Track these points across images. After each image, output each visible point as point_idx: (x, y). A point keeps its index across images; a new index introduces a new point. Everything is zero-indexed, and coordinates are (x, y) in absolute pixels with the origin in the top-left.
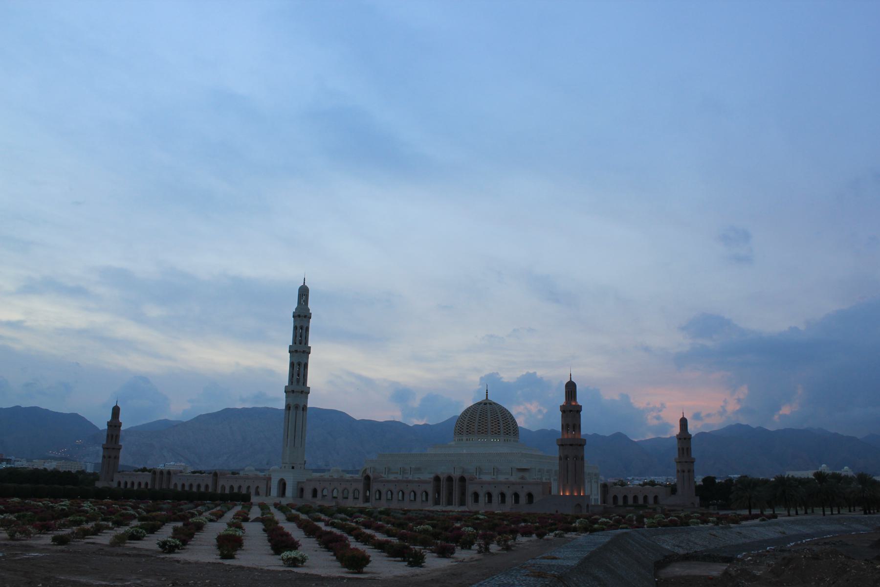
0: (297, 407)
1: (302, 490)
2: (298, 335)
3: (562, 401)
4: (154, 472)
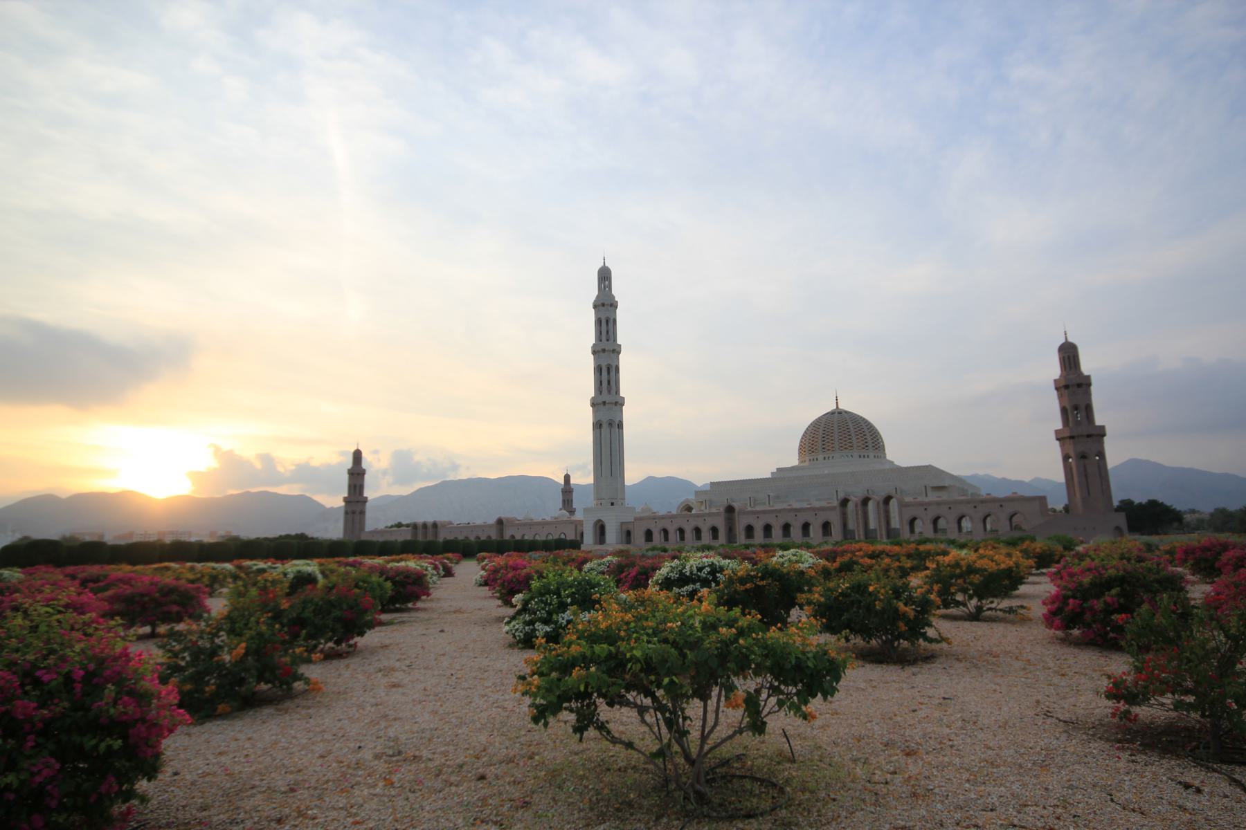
1: (629, 533)
4: (415, 526)
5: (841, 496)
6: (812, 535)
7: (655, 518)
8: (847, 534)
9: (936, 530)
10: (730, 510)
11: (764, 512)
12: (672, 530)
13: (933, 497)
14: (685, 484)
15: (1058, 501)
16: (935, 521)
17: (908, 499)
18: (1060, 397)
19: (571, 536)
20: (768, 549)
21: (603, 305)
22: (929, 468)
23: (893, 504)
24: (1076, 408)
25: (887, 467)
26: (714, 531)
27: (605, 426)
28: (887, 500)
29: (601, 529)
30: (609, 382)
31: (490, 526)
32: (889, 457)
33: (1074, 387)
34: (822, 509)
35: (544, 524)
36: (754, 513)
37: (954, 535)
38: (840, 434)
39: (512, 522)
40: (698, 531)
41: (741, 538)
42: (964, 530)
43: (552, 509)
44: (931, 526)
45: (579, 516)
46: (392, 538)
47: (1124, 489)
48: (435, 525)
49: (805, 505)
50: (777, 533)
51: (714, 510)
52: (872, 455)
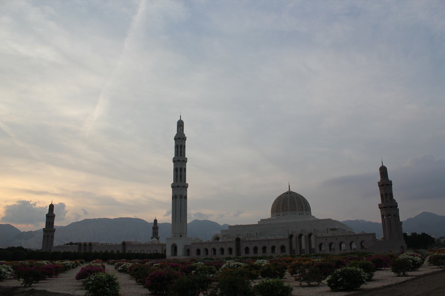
0: (181, 197)
1: (188, 250)
2: (179, 152)
3: (379, 179)
4: (80, 244)
5: (290, 233)
6: (276, 252)
7: (201, 243)
8: (292, 251)
9: (330, 249)
10: (238, 240)
11: (254, 241)
12: (210, 249)
13: (330, 234)
14: (214, 225)
15: (380, 236)
16: (330, 245)
17: (319, 235)
18: (380, 189)
19: (160, 252)
20: (255, 259)
21: (179, 139)
22: (329, 220)
23: (312, 237)
24: (386, 194)
25: (312, 219)
26: (230, 250)
27: (178, 197)
28: (310, 235)
29: (175, 248)
30: (181, 176)
31: (119, 245)
32: (313, 214)
33: (385, 185)
34: (281, 240)
35: (140, 245)
36: (249, 241)
37: (318, 251)
38: (290, 203)
39: (130, 244)
40: (222, 250)
41: (243, 254)
42: (342, 249)
43: (145, 238)
44: (329, 247)
45: (162, 241)
46: (67, 250)
47: (407, 230)
48: (90, 244)
49: (273, 238)
50: (260, 251)
51: (230, 240)
52: (304, 213)
